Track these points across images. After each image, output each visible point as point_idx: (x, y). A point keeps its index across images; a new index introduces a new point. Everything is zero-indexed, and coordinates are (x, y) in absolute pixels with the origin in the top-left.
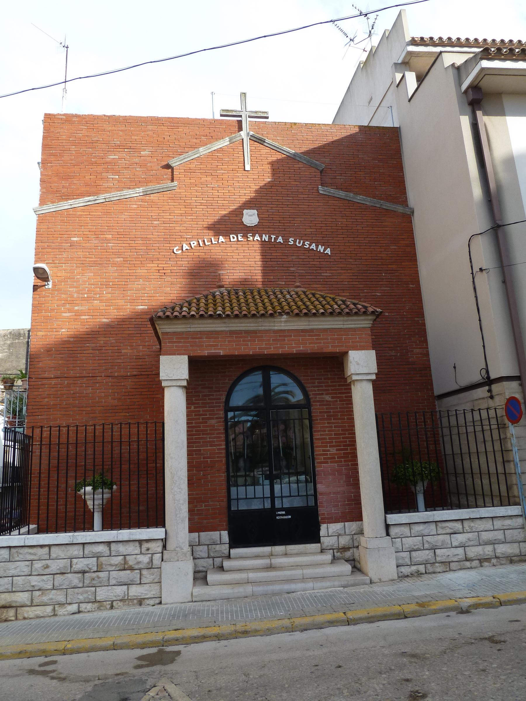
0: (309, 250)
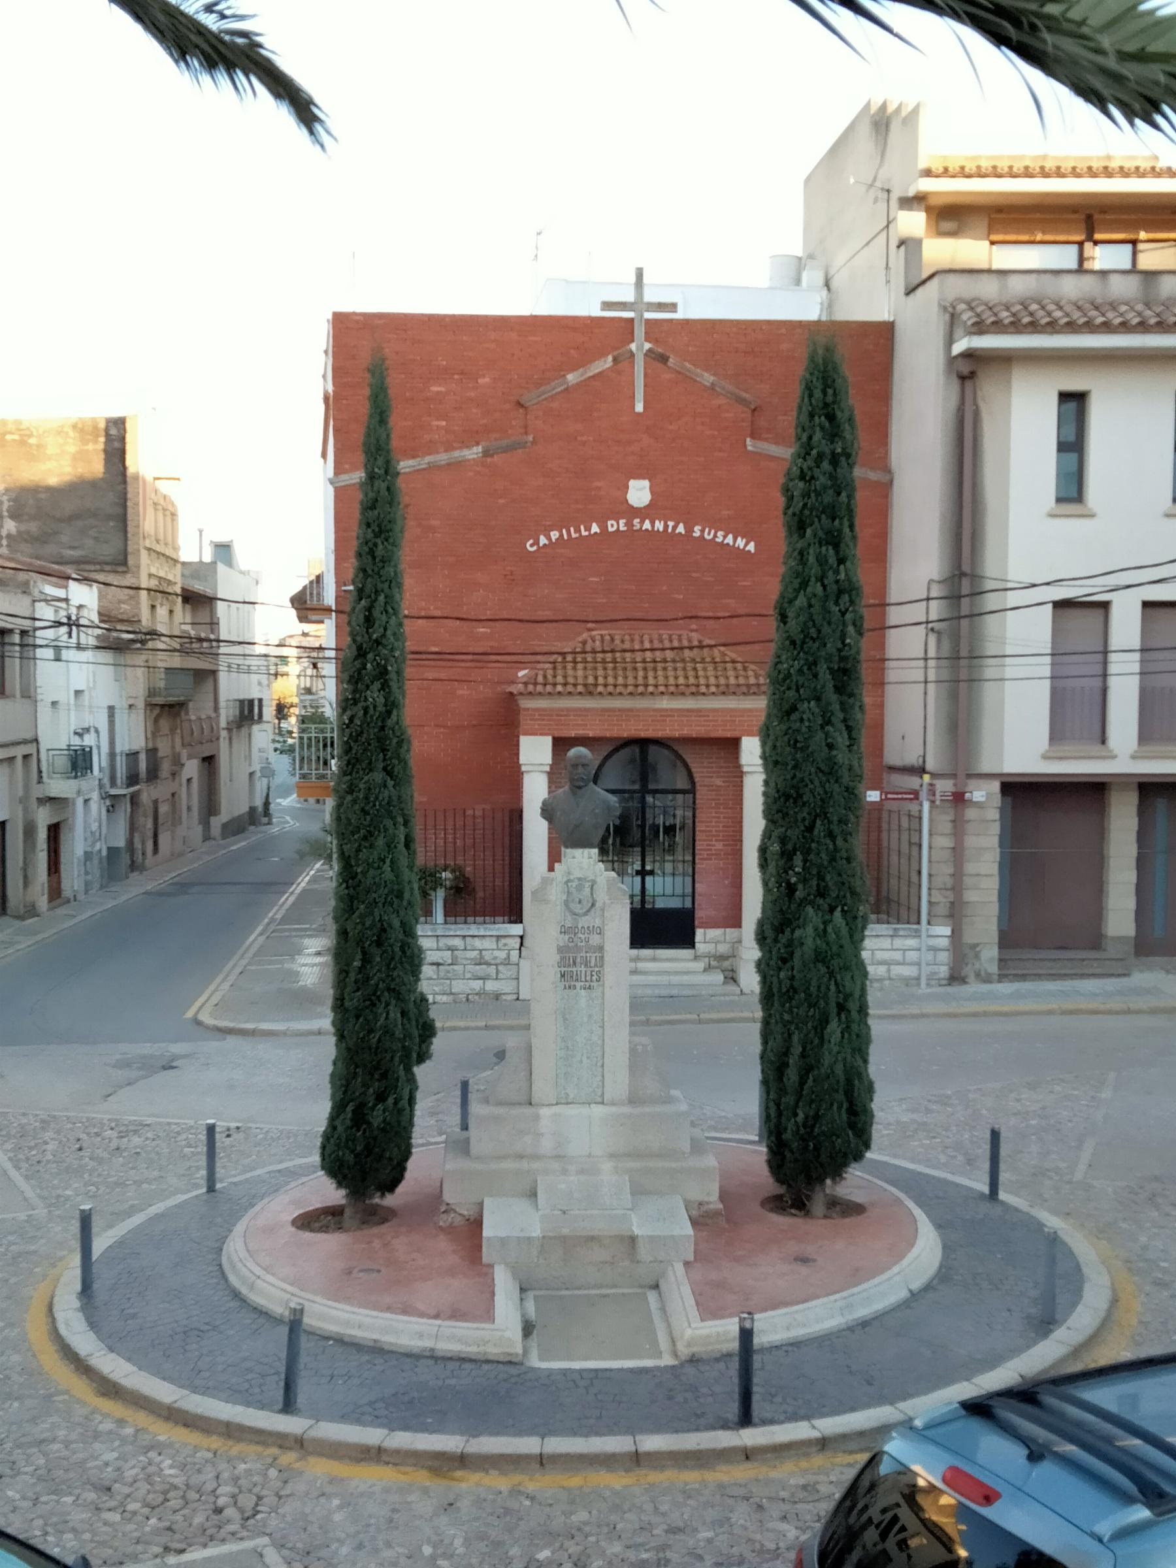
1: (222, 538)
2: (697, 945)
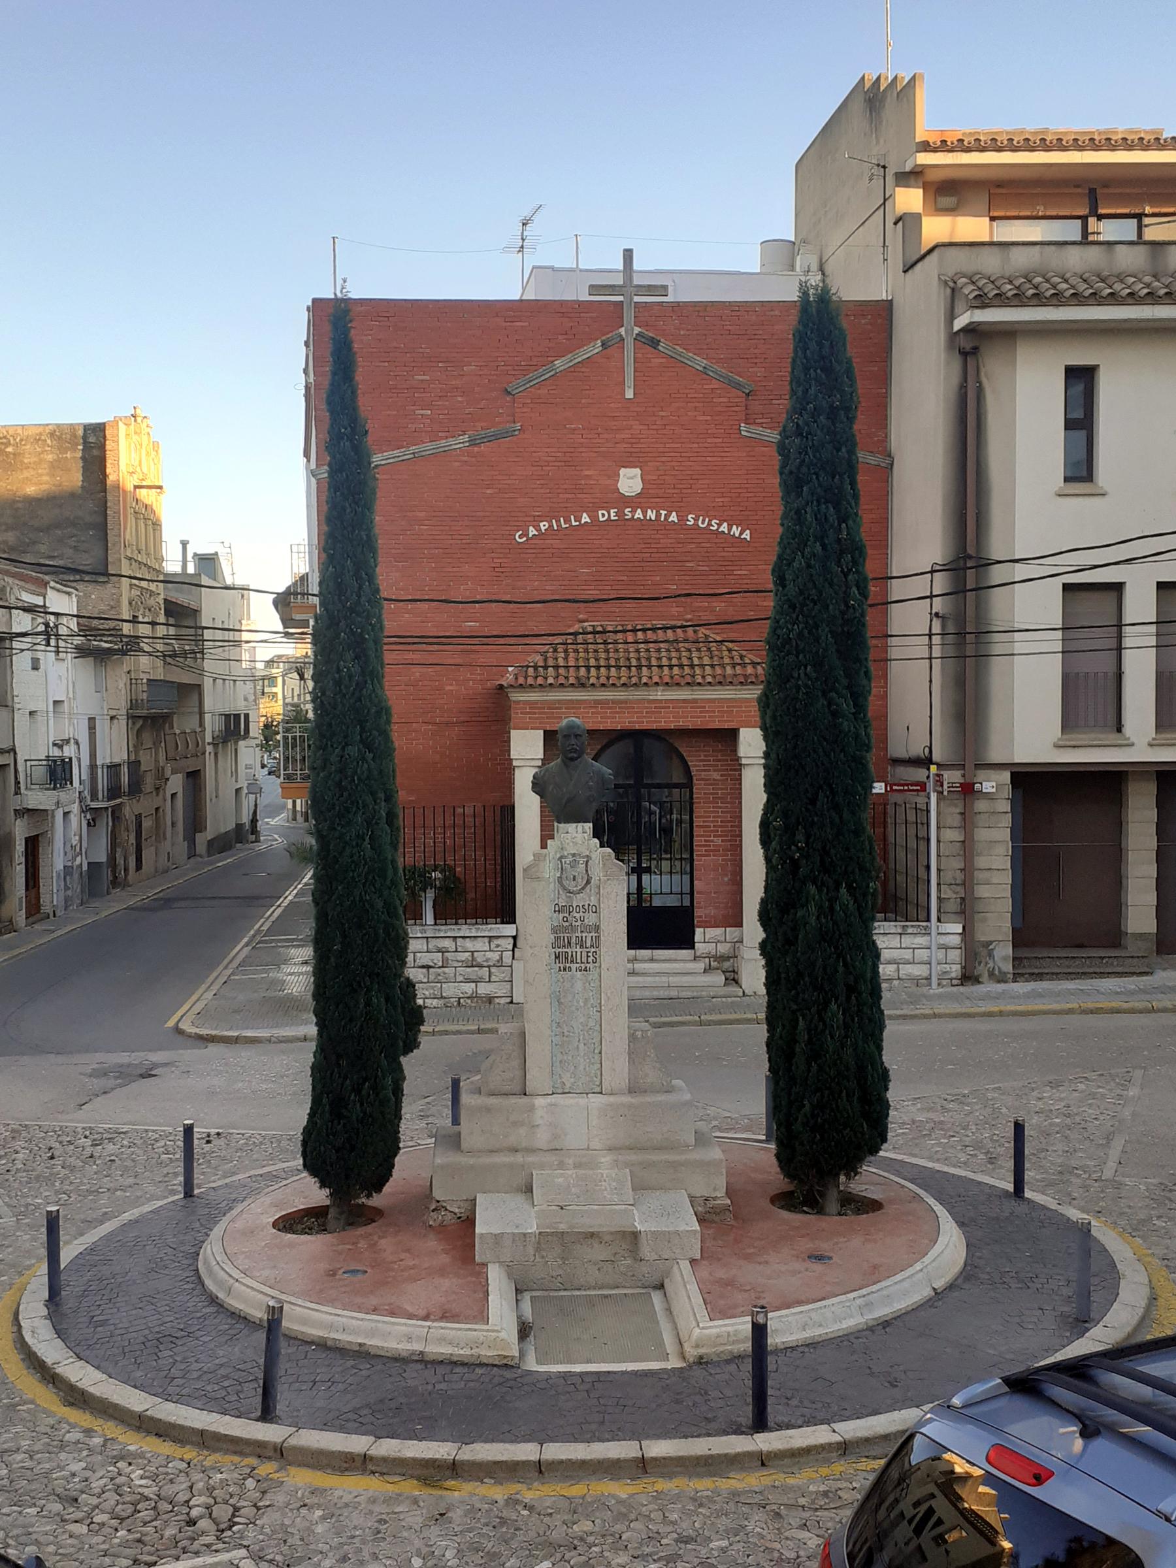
0: (717, 533)
1: (206, 549)
2: (697, 945)
